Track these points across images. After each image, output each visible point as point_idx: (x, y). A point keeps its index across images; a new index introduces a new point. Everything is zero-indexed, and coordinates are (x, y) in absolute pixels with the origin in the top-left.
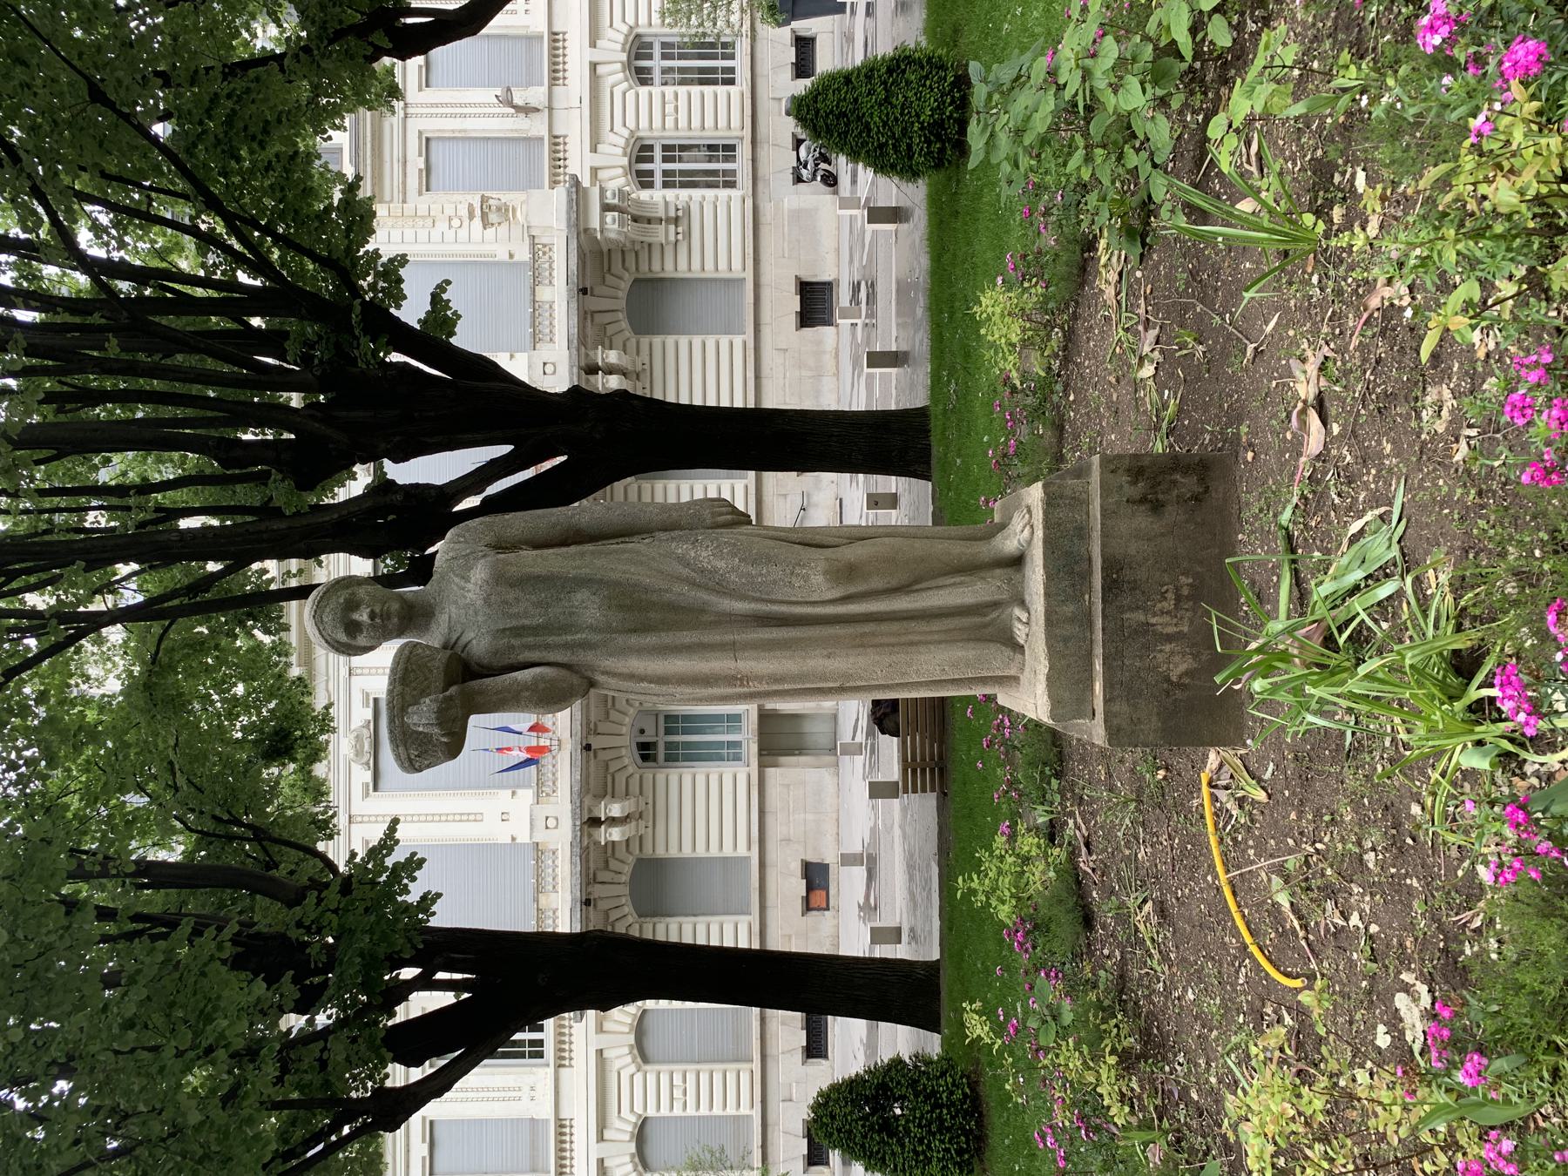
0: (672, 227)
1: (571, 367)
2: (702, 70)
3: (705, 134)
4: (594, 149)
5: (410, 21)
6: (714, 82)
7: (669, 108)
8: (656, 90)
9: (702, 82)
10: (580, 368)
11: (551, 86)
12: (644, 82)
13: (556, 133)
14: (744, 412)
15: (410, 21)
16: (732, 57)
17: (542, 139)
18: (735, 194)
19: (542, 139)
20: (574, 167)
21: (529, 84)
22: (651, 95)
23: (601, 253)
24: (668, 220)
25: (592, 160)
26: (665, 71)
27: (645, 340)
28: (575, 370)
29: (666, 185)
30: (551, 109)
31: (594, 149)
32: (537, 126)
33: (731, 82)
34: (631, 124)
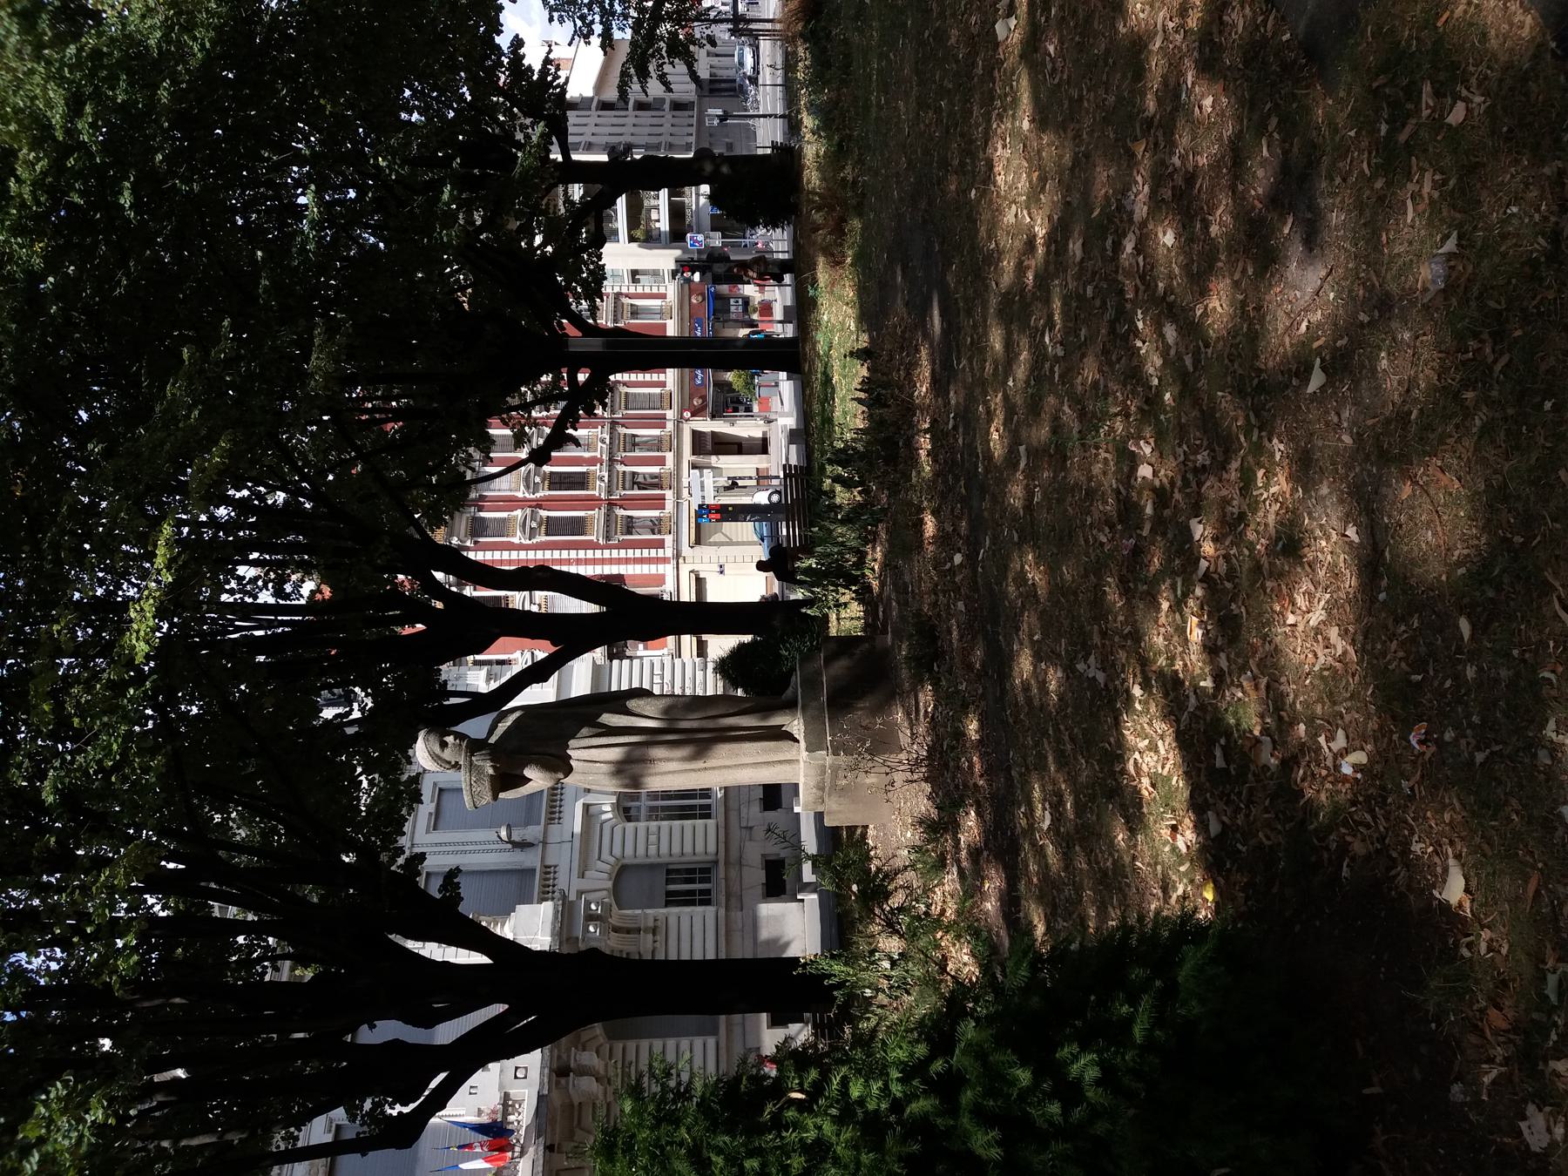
0: (650, 936)
1: (542, 1068)
2: (682, 808)
3: (683, 859)
4: (582, 875)
5: (453, 701)
6: (693, 817)
7: (653, 838)
8: (642, 825)
9: (681, 817)
10: (551, 1070)
11: (547, 825)
12: (629, 819)
13: (548, 863)
14: (716, 962)
15: (453, 701)
16: (708, 880)
17: (533, 870)
18: (711, 822)
19: (533, 870)
20: (562, 883)
21: (527, 824)
22: (624, 1049)
23: (572, 1105)
24: (646, 931)
25: (577, 884)
26: (652, 809)
27: (619, 1046)
28: (546, 1071)
29: (649, 819)
30: (545, 843)
31: (582, 875)
32: (530, 859)
33: (708, 816)
34: (617, 851)
